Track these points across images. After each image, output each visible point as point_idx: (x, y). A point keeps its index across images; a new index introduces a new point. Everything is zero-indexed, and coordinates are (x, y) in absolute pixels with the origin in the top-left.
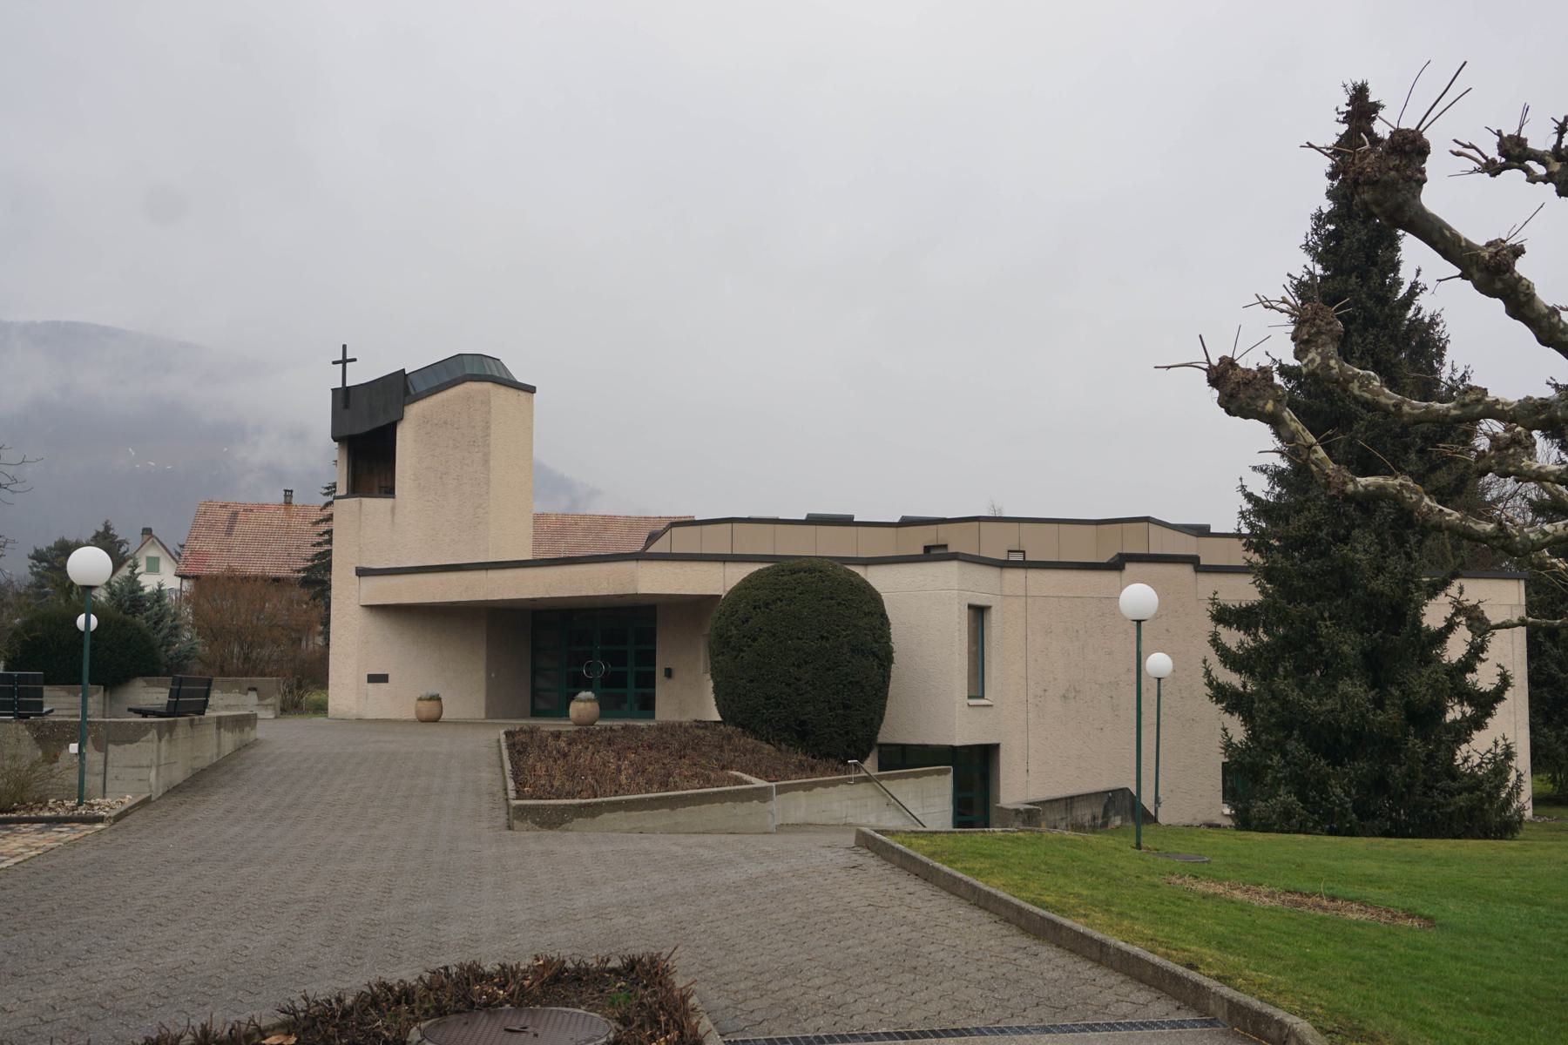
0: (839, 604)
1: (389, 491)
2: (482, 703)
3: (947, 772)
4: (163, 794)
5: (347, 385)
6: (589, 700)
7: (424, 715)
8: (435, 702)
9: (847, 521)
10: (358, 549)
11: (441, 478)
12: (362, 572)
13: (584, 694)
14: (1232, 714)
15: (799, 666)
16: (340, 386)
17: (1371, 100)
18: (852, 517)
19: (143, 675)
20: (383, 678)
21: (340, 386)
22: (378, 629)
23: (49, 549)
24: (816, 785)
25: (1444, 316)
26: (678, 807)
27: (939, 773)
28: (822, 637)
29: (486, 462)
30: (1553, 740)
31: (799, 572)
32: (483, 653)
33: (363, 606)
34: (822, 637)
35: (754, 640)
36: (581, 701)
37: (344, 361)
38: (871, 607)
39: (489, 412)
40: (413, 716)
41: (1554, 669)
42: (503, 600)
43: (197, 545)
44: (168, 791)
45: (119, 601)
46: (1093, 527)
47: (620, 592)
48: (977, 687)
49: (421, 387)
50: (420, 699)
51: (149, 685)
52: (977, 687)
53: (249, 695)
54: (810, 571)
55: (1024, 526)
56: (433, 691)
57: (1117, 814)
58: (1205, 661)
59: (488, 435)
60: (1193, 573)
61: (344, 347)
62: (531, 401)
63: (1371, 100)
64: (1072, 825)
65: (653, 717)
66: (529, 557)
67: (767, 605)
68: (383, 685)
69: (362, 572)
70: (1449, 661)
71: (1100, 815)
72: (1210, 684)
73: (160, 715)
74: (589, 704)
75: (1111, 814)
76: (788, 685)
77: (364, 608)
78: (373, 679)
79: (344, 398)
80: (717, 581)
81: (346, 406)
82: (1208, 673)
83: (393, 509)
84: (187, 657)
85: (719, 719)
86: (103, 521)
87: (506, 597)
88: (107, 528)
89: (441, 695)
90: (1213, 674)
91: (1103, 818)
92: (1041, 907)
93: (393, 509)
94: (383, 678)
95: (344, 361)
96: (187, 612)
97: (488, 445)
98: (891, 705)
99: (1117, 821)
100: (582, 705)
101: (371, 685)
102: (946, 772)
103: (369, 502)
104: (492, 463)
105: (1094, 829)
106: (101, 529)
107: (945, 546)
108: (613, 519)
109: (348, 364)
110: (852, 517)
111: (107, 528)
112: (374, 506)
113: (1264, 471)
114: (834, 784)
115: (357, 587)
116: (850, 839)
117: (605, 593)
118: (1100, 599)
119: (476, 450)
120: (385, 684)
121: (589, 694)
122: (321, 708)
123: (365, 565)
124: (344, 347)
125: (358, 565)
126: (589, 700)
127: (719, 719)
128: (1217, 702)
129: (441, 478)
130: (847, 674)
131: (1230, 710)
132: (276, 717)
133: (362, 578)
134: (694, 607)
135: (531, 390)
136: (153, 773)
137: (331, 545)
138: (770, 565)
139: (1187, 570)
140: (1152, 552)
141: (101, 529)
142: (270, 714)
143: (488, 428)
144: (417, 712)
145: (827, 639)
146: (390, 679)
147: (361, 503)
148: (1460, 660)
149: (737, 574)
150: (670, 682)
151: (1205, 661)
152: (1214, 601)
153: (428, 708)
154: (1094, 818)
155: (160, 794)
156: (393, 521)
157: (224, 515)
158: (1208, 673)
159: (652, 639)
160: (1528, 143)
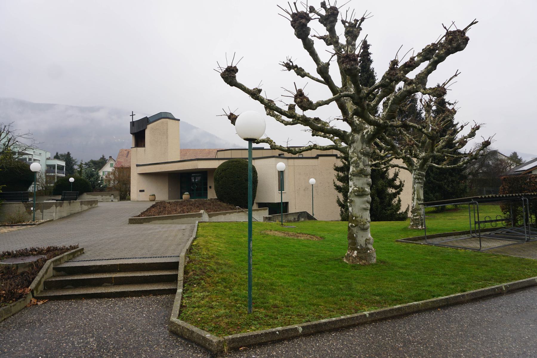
0: (242, 169)
1: (144, 146)
2: (168, 196)
3: (267, 209)
4: (58, 219)
5: (133, 121)
6: (187, 194)
7: (151, 199)
8: (153, 196)
12: (137, 166)
13: (186, 193)
14: (340, 193)
15: (232, 185)
16: (132, 121)
17: (368, 44)
18: (264, 148)
19: (86, 192)
20: (143, 191)
22: (142, 179)
23: (89, 162)
24: (227, 213)
27: (264, 209)
28: (238, 177)
29: (167, 138)
30: (432, 197)
32: (167, 184)
33: (140, 174)
35: (222, 179)
36: (185, 195)
37: (133, 115)
39: (168, 126)
40: (149, 200)
41: (432, 179)
42: (168, 171)
43: (119, 160)
44: (60, 218)
45: (88, 175)
48: (281, 187)
49: (151, 121)
50: (150, 196)
51: (87, 194)
52: (281, 187)
54: (236, 161)
56: (153, 194)
57: (302, 218)
58: (333, 180)
60: (336, 159)
63: (368, 44)
64: (287, 221)
65: (207, 198)
66: (179, 160)
67: (225, 170)
68: (143, 192)
69: (137, 166)
71: (297, 218)
72: (335, 186)
73: (60, 200)
74: (187, 195)
75: (300, 218)
76: (230, 189)
78: (141, 191)
79: (133, 124)
80: (215, 165)
81: (133, 126)
82: (334, 183)
83: (145, 150)
84: (104, 187)
85: (217, 198)
86: (102, 155)
87: (169, 170)
88: (103, 156)
89: (156, 195)
90: (336, 183)
91: (298, 219)
93: (145, 150)
94: (143, 191)
95: (133, 115)
96: (43, 176)
99: (303, 219)
100: (185, 196)
101: (140, 192)
102: (266, 209)
103: (139, 149)
104: (168, 138)
105: (294, 221)
106: (102, 157)
108: (190, 150)
110: (264, 148)
111: (103, 156)
112: (140, 149)
114: (232, 213)
117: (191, 168)
122: (129, 199)
123: (138, 164)
127: (217, 198)
128: (337, 190)
130: (244, 186)
131: (340, 192)
132: (118, 201)
134: (212, 170)
135: (179, 120)
136: (54, 214)
138: (227, 160)
139: (334, 158)
141: (102, 157)
142: (117, 201)
143: (168, 130)
144: (149, 199)
145: (239, 178)
148: (392, 178)
149: (221, 162)
151: (333, 180)
152: (335, 166)
153: (152, 198)
154: (295, 219)
155: (57, 219)
156: (145, 153)
157: (126, 152)
158: (334, 183)
159: (207, 180)
160: (237, 75)
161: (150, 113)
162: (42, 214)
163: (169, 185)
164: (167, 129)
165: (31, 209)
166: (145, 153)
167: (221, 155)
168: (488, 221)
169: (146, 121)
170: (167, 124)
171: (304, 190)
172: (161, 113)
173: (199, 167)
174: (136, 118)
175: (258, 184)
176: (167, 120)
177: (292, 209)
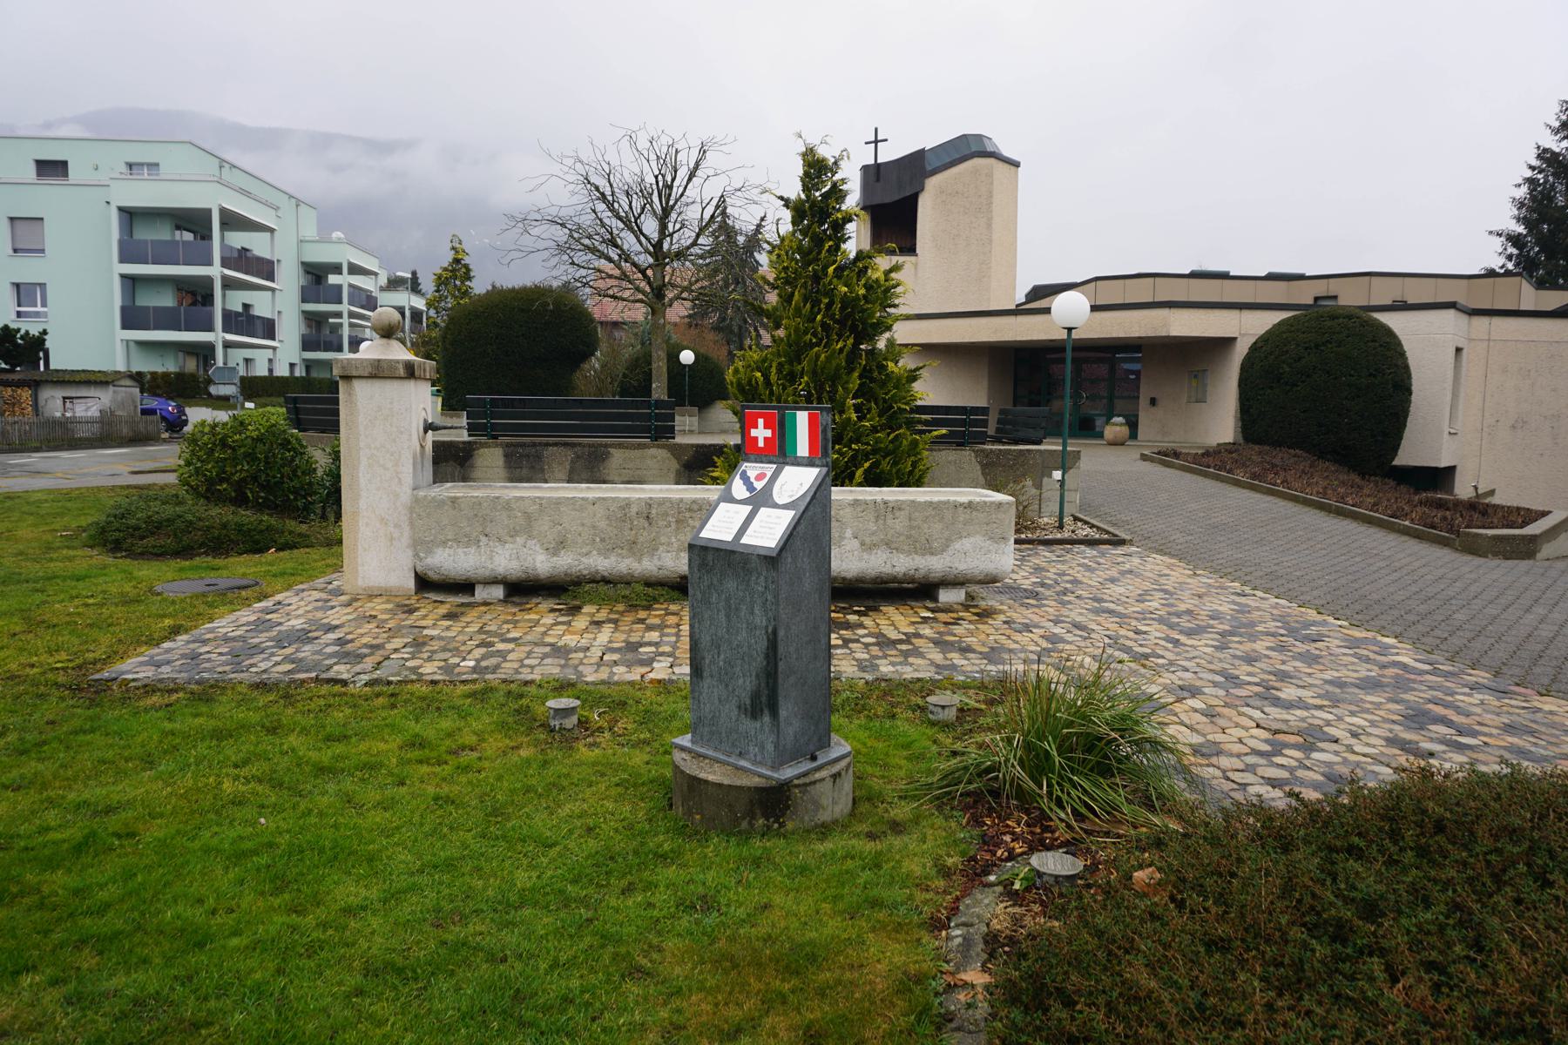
6: (1121, 425)
9: (1224, 276)
25: (813, 140)
28: (1371, 375)
29: (989, 226)
31: (1337, 318)
32: (985, 383)
34: (1371, 375)
37: (876, 142)
38: (1390, 346)
39: (992, 183)
46: (1465, 282)
47: (1151, 334)
55: (1407, 279)
62: (1016, 174)
74: (1118, 428)
92: (307, 671)
95: (876, 142)
98: (1407, 433)
107: (1335, 297)
113: (1500, 235)
116: (498, 592)
118: (1551, 343)
121: (1120, 420)
126: (1121, 425)
135: (1016, 164)
140: (1522, 308)
145: (1375, 376)
150: (1153, 409)
156: (916, 275)
161: (930, 139)
162: (1038, 492)
163: (990, 388)
164: (990, 195)
165: (1057, 469)
166: (916, 275)
167: (1277, 293)
168: (87, 439)
169: (917, 167)
170: (990, 175)
171: (1514, 427)
172: (964, 138)
173: (1174, 333)
174: (888, 154)
175: (1414, 398)
176: (992, 161)
177: (1463, 489)
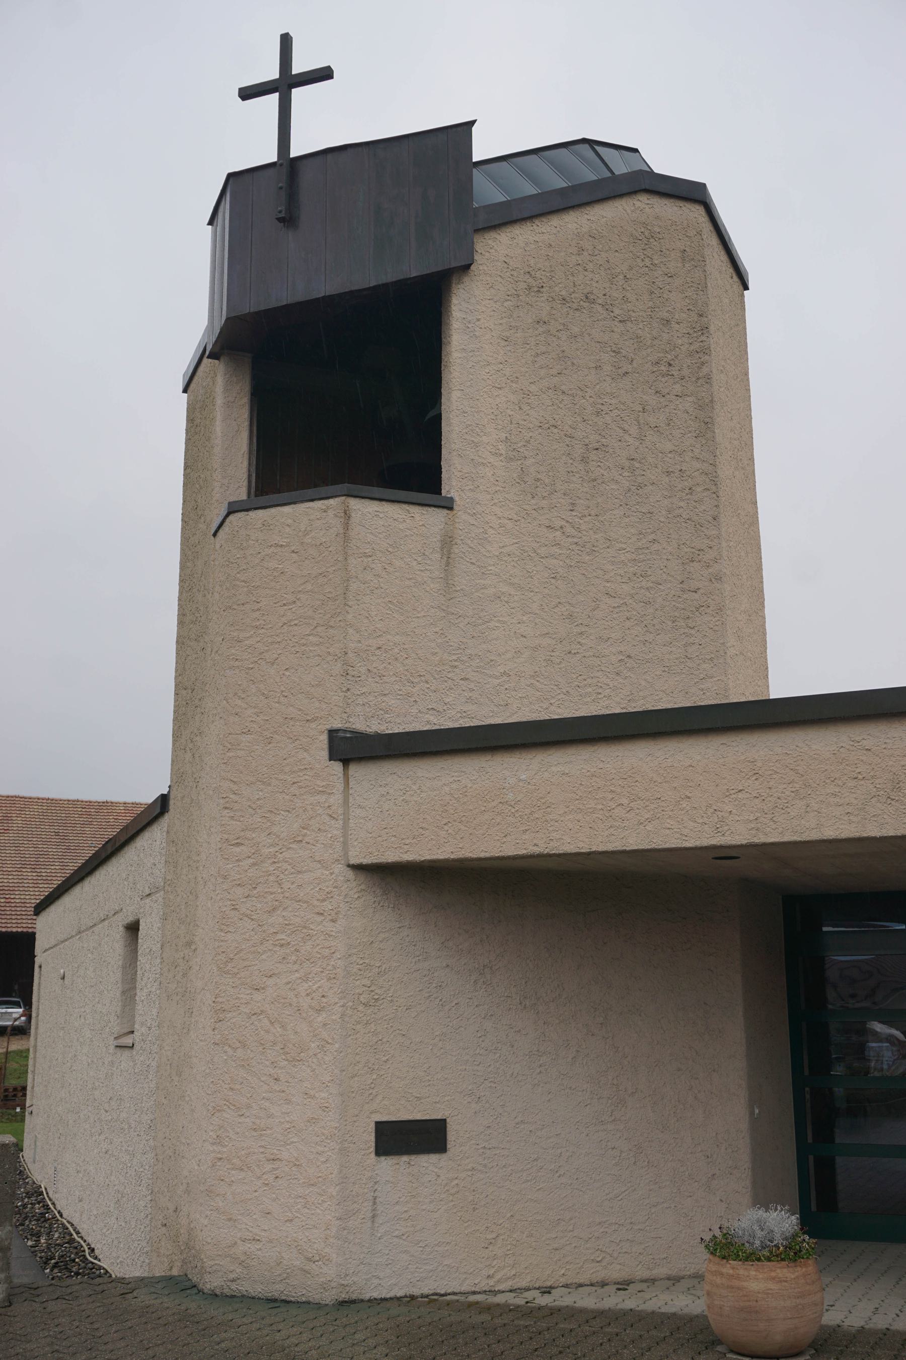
5: (294, 152)
10: (338, 668)
11: (584, 460)
21: (274, 158)
26: (680, 1315)
29: (707, 425)
33: (359, 868)
53: (453, 494)
59: (705, 351)
61: (286, 41)
68: (426, 1162)
70: (116, 1276)
77: (362, 877)
83: (447, 543)
93: (447, 543)
97: (708, 378)
101: (387, 1163)
109: (297, 93)
115: (336, 799)
119: (678, 388)
120: (433, 1158)
124: (286, 41)
125: (337, 724)
129: (584, 460)
133: (355, 770)
137: (27, 1001)
143: (705, 329)
146: (451, 1136)
147: (347, 514)
